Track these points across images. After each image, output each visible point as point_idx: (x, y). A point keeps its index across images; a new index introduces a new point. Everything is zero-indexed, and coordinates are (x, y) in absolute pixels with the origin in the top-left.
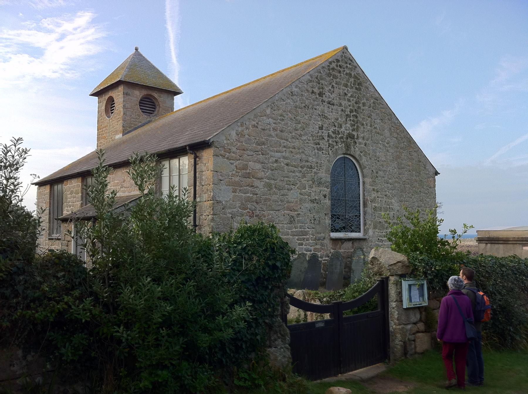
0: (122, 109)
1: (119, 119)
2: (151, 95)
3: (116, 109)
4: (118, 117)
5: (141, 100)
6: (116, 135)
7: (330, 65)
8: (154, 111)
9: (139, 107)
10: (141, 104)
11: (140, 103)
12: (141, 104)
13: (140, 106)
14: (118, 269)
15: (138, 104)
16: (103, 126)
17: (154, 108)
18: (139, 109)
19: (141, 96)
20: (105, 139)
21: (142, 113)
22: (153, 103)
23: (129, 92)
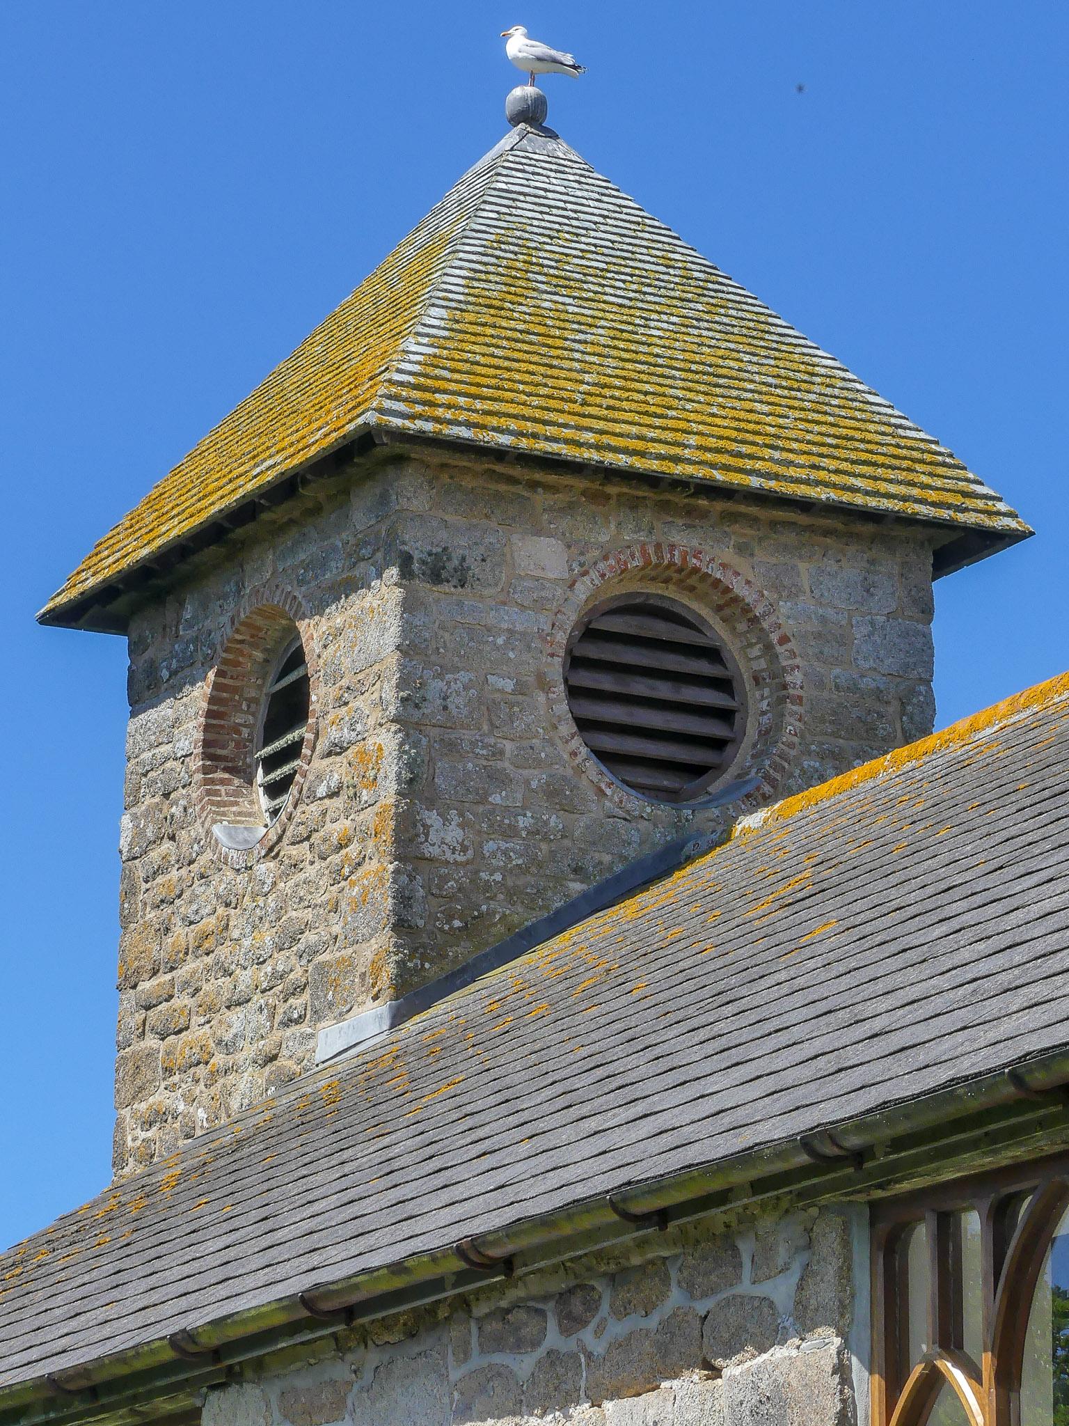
0: (387, 740)
1: (353, 850)
2: (689, 577)
3: (322, 745)
4: (344, 824)
5: (590, 634)
6: (318, 1015)
7: (202, 1083)
8: (718, 744)
9: (563, 708)
10: (586, 679)
11: (575, 662)
12: (586, 679)
13: (574, 692)
14: (792, 638)
15: (555, 669)
16: (179, 930)
17: (726, 715)
18: (568, 728)
19: (583, 591)
20: (201, 1071)
21: (593, 767)
22: (713, 654)
23: (460, 545)
